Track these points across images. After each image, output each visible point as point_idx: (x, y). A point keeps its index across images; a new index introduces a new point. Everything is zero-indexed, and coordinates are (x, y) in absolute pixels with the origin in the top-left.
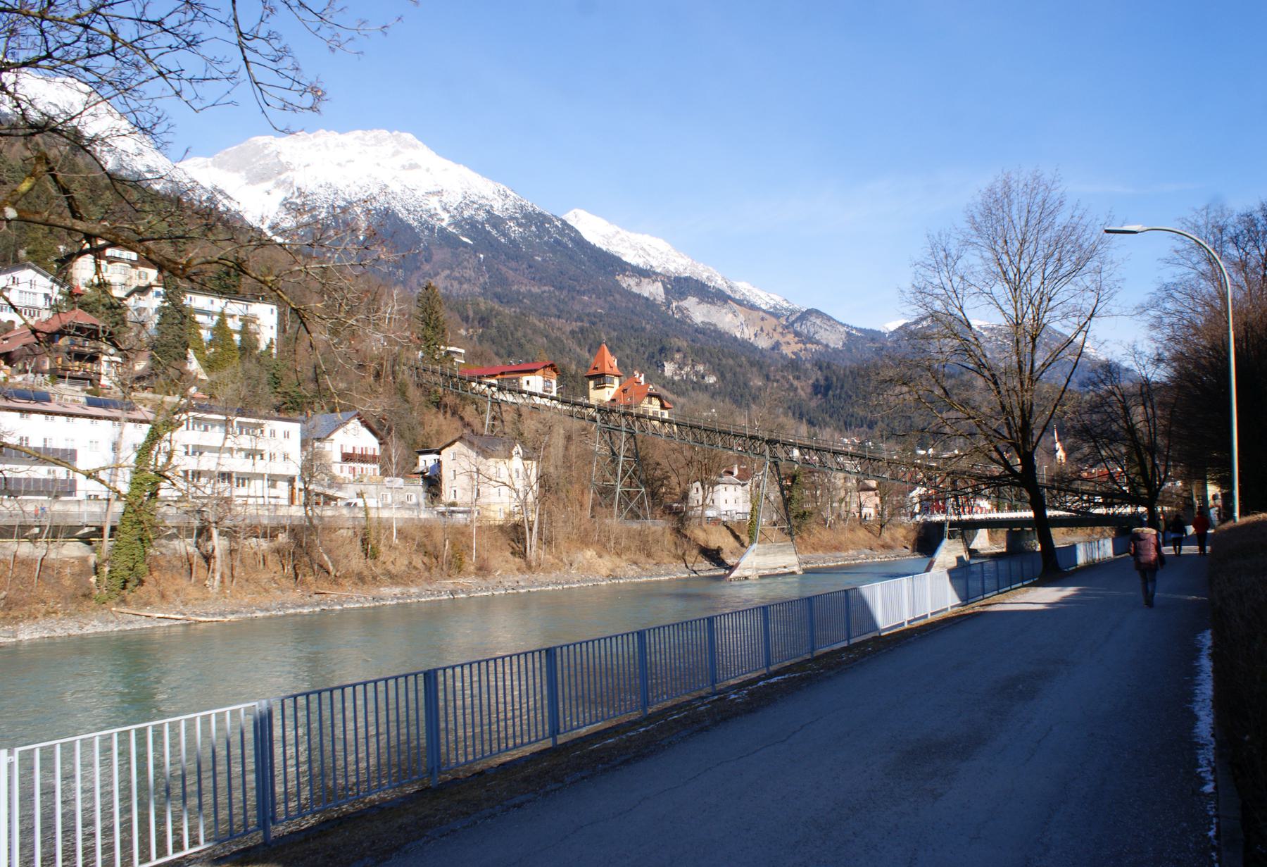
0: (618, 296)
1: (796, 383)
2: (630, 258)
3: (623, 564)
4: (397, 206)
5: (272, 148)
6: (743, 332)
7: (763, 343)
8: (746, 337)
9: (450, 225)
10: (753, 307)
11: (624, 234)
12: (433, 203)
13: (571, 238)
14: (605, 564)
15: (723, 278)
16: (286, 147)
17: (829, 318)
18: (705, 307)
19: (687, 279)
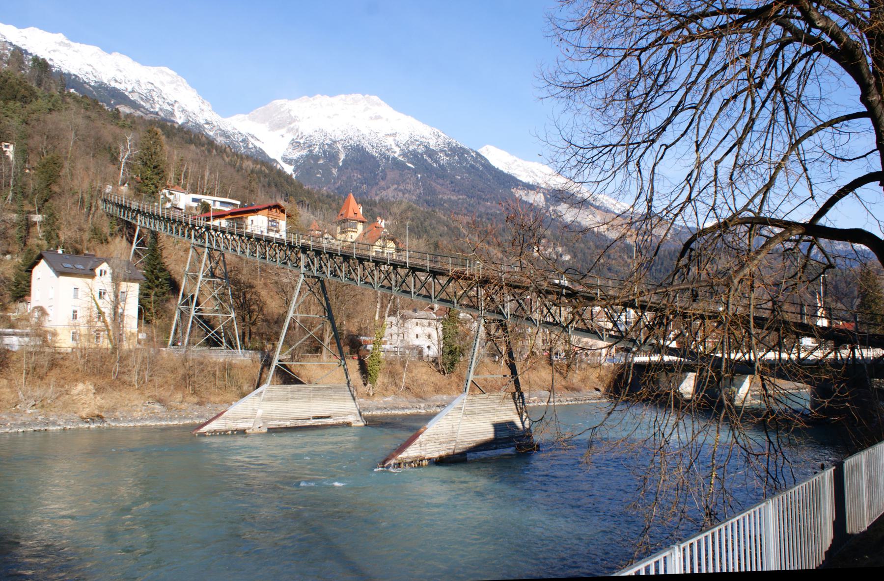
2: (524, 178)
4: (365, 144)
11: (520, 162)
12: (390, 142)
13: (482, 164)
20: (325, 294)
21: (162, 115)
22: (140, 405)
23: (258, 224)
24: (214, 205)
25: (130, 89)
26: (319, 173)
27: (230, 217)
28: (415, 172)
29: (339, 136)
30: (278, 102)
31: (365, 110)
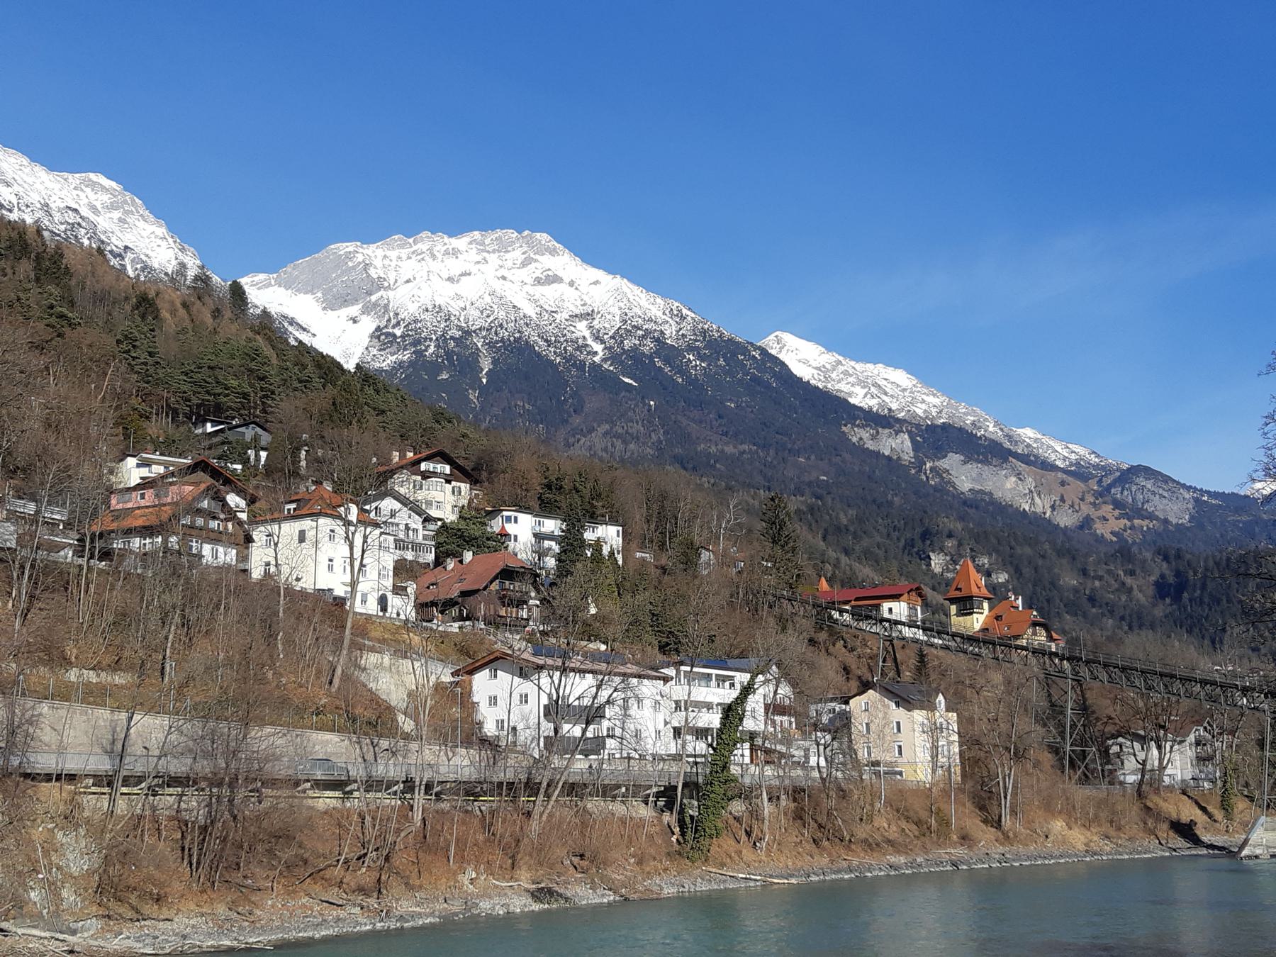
0: (847, 456)
1: (1129, 581)
2: (859, 398)
3: (1095, 838)
5: (360, 258)
6: (1033, 503)
7: (1065, 519)
8: (1039, 510)
9: (605, 360)
10: (1047, 466)
11: (849, 364)
12: (582, 329)
13: (775, 374)
14: (1078, 838)
15: (996, 424)
16: (381, 257)
17: (1167, 479)
18: (973, 468)
19: (945, 427)
29: (476, 320)
30: (350, 247)
31: (524, 264)
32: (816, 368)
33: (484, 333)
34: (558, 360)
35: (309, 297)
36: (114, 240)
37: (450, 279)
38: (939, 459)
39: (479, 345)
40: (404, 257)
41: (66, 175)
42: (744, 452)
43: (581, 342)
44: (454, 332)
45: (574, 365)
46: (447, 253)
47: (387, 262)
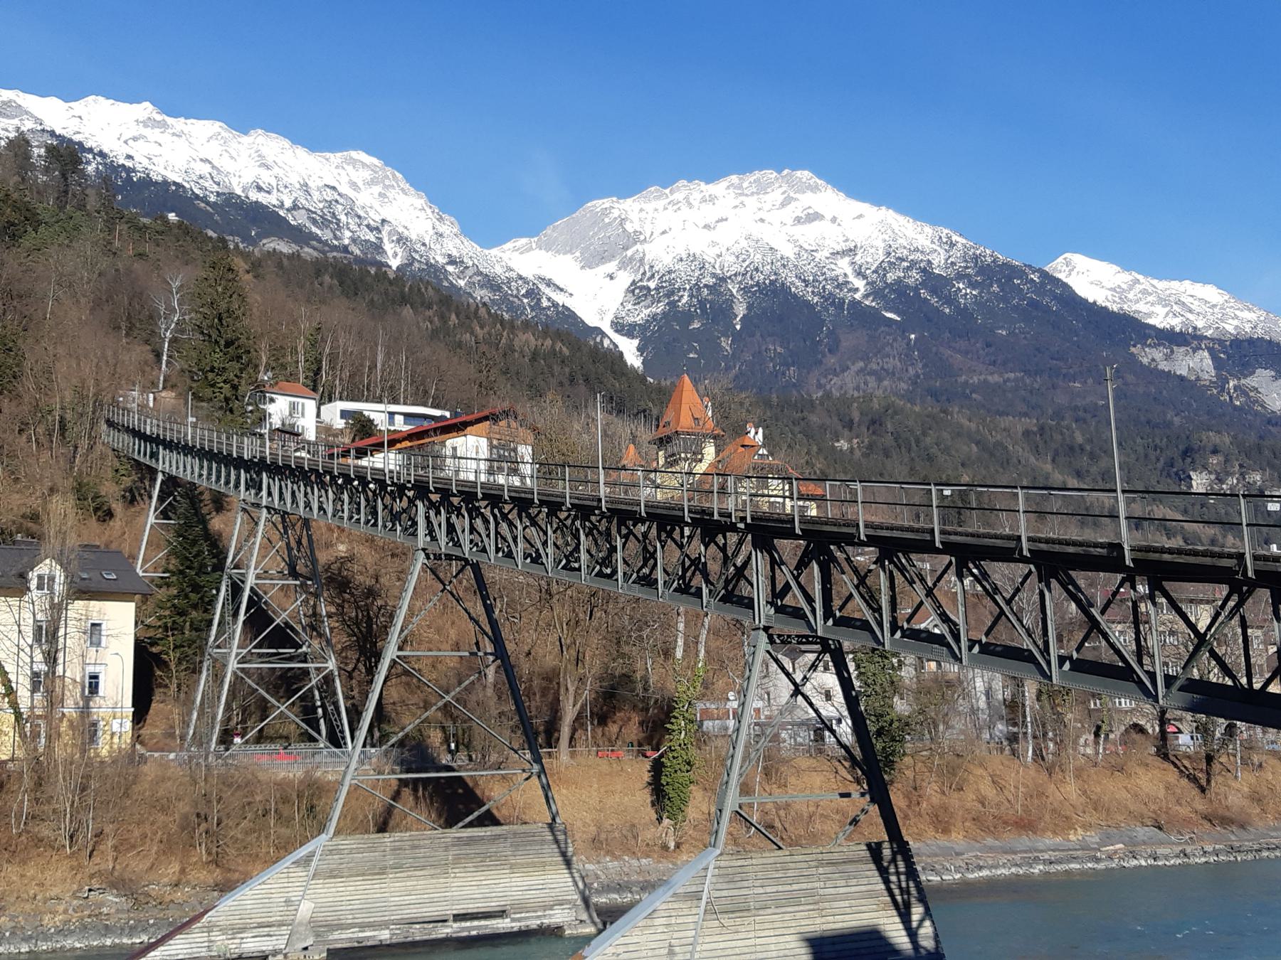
2: (1160, 318)
4: (790, 278)
5: (616, 213)
9: (866, 296)
11: (1145, 282)
12: (843, 267)
13: (1055, 297)
16: (636, 211)
19: (1251, 342)
20: (485, 598)
21: (357, 252)
22: (67, 897)
23: (468, 455)
24: (391, 422)
25: (288, 204)
26: (692, 349)
27: (407, 444)
28: (903, 328)
29: (731, 265)
30: (606, 203)
31: (783, 205)
32: (1111, 289)
33: (739, 278)
34: (816, 299)
35: (569, 256)
36: (372, 214)
37: (707, 227)
38: (1245, 377)
39: (734, 291)
40: (661, 208)
41: (328, 155)
42: (1008, 380)
43: (841, 280)
44: (710, 281)
45: (833, 303)
46: (703, 200)
47: (643, 215)
